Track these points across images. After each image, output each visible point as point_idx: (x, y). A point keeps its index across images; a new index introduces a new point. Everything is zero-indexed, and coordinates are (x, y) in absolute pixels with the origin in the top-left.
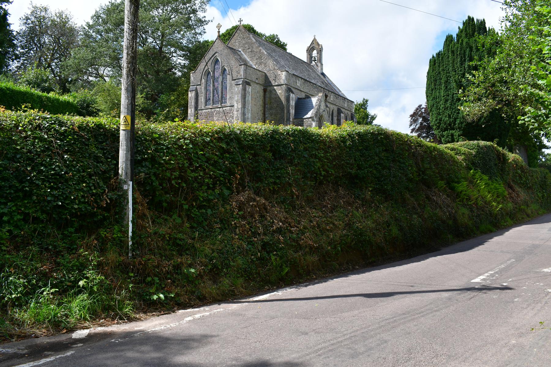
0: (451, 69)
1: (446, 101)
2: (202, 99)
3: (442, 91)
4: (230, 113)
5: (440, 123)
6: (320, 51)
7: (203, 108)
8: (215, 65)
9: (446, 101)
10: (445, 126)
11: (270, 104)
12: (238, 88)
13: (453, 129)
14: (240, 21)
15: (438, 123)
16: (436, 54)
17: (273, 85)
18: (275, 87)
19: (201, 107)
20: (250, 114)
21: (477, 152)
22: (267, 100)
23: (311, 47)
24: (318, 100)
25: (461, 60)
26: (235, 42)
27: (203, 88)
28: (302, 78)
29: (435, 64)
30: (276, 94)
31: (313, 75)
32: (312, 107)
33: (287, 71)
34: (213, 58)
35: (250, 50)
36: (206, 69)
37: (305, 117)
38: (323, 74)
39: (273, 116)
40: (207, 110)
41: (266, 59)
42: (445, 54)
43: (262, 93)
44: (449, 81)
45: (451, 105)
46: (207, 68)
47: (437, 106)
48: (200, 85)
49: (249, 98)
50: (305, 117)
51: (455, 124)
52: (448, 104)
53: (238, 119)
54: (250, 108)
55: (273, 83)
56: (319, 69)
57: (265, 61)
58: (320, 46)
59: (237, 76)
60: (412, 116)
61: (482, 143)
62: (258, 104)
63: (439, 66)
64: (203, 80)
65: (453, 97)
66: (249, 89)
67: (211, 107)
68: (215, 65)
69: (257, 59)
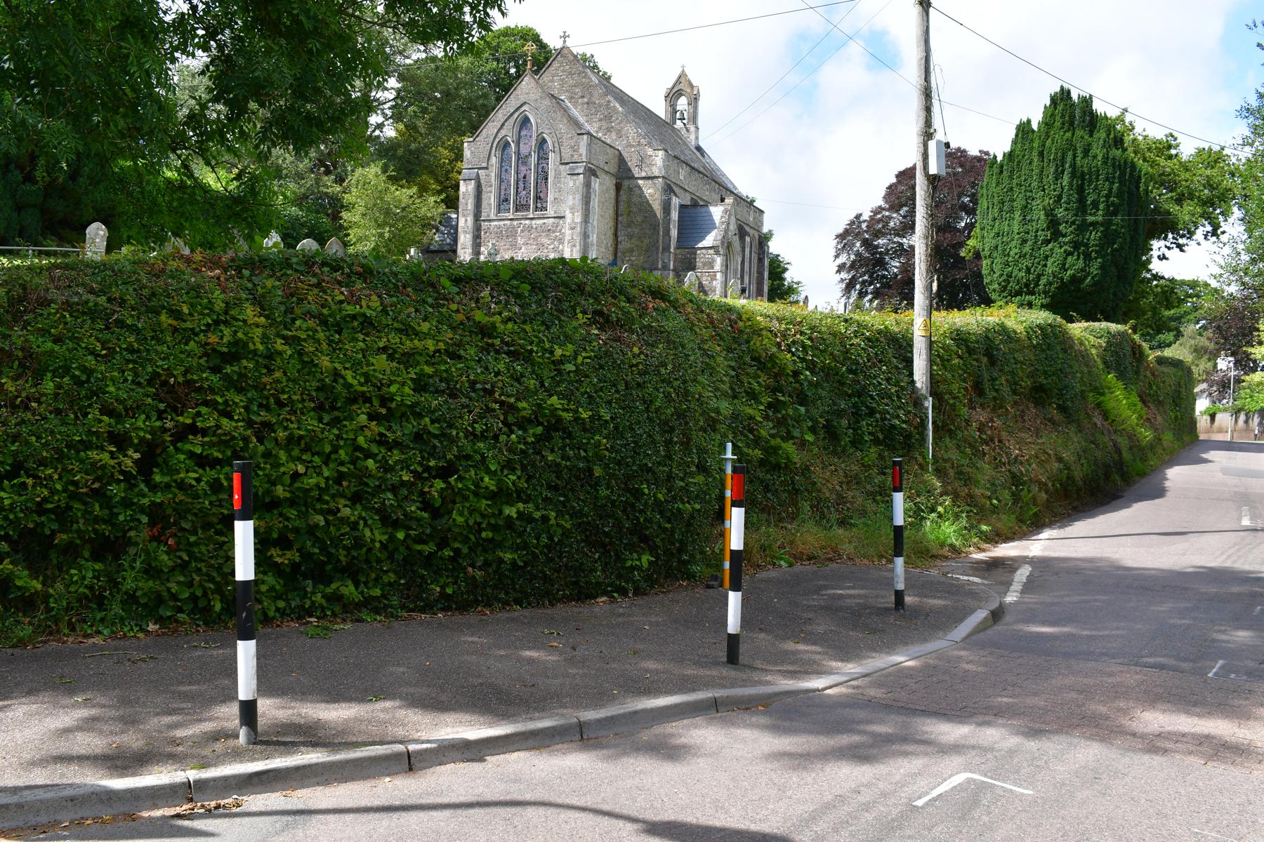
0: (1035, 184)
1: (1024, 241)
2: (490, 199)
3: (1015, 222)
4: (554, 232)
5: (1007, 281)
6: (694, 101)
7: (492, 216)
8: (521, 129)
9: (1024, 241)
10: (1017, 287)
11: (629, 215)
12: (575, 181)
13: (1032, 293)
14: (565, 36)
15: (1004, 281)
16: (1004, 154)
17: (636, 176)
18: (640, 182)
19: (489, 216)
20: (595, 236)
21: (1108, 342)
22: (622, 207)
23: (676, 90)
24: (726, 211)
25: (1057, 170)
26: (552, 81)
27: (493, 175)
28: (687, 164)
29: (1001, 172)
30: (642, 195)
31: (687, 152)
32: (712, 226)
33: (666, 151)
34: (517, 114)
35: (586, 100)
36: (500, 136)
37: (700, 245)
38: (699, 148)
39: (634, 240)
40: (502, 223)
41: (621, 121)
42: (1024, 155)
43: (613, 193)
44: (1029, 206)
45: (1033, 250)
46: (503, 133)
47: (1004, 250)
48: (486, 168)
49: (595, 203)
50: (700, 245)
51: (1037, 285)
52: (1027, 249)
53: (575, 246)
54: (595, 223)
55: (636, 172)
56: (692, 137)
57: (618, 127)
58: (695, 89)
59: (572, 156)
60: (841, 237)
61: (1114, 327)
62: (607, 216)
63: (1011, 177)
64: (493, 160)
65: (1036, 236)
66: (596, 184)
67: (511, 217)
68: (521, 129)
69: (600, 120)
